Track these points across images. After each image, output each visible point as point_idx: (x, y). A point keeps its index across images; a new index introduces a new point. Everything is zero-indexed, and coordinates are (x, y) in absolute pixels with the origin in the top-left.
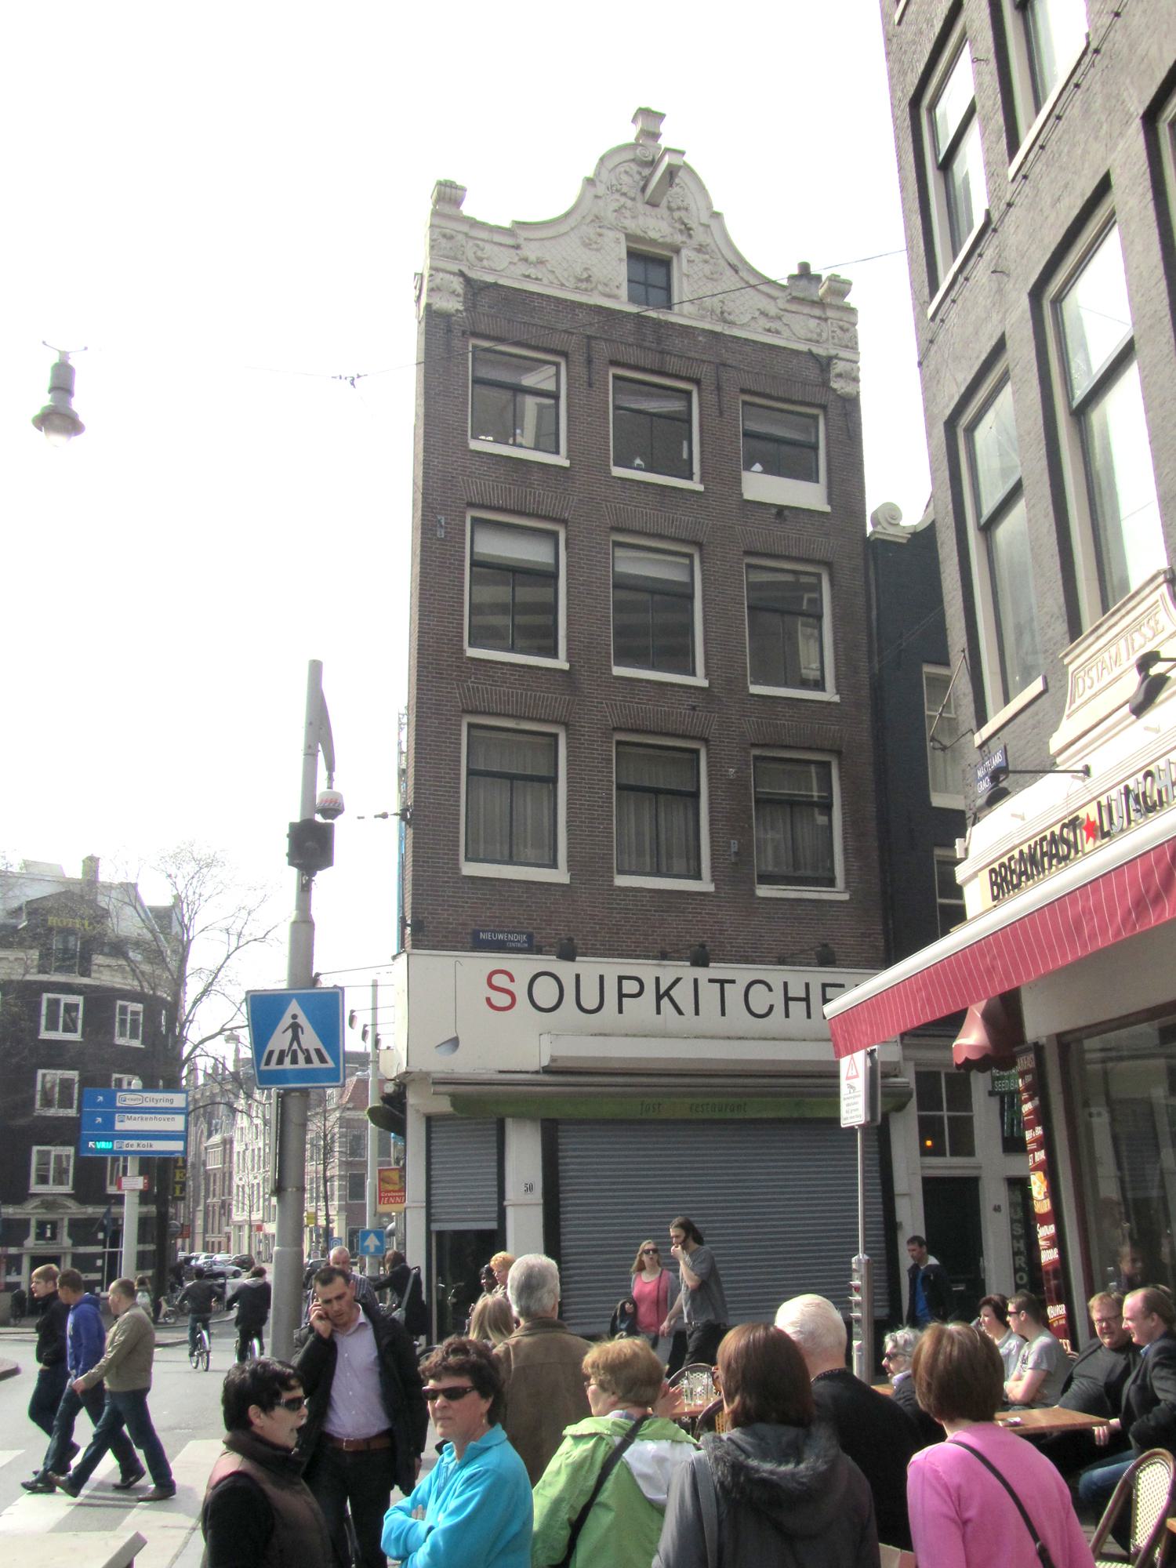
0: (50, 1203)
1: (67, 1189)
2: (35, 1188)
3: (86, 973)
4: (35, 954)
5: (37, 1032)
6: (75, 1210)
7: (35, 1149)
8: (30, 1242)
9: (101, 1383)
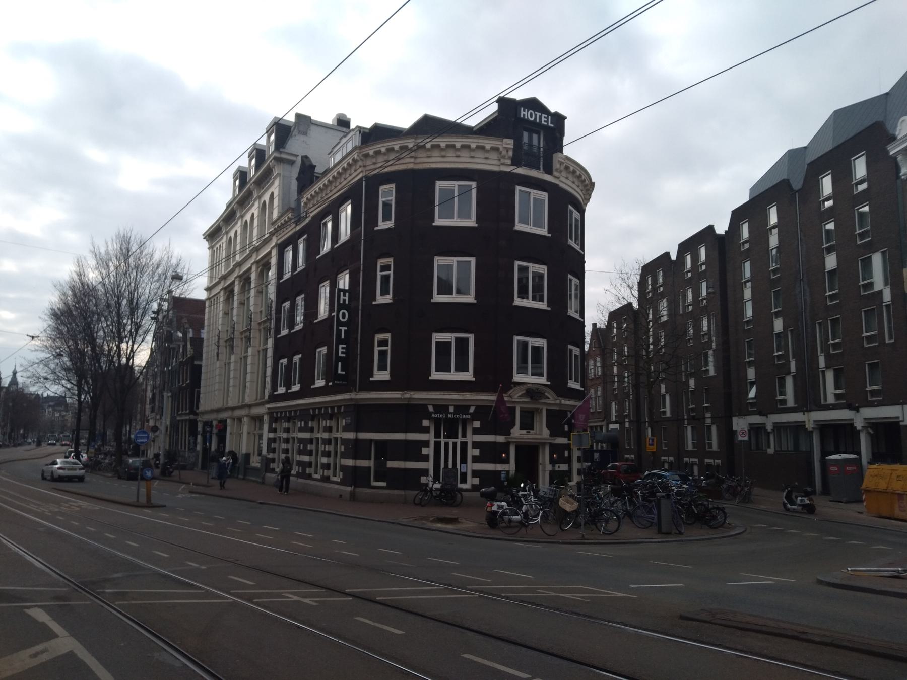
0: (533, 393)
1: (542, 380)
2: (517, 378)
3: (549, 170)
4: (509, 143)
5: (514, 225)
6: (552, 399)
7: (516, 338)
8: (517, 432)
9: (469, 406)
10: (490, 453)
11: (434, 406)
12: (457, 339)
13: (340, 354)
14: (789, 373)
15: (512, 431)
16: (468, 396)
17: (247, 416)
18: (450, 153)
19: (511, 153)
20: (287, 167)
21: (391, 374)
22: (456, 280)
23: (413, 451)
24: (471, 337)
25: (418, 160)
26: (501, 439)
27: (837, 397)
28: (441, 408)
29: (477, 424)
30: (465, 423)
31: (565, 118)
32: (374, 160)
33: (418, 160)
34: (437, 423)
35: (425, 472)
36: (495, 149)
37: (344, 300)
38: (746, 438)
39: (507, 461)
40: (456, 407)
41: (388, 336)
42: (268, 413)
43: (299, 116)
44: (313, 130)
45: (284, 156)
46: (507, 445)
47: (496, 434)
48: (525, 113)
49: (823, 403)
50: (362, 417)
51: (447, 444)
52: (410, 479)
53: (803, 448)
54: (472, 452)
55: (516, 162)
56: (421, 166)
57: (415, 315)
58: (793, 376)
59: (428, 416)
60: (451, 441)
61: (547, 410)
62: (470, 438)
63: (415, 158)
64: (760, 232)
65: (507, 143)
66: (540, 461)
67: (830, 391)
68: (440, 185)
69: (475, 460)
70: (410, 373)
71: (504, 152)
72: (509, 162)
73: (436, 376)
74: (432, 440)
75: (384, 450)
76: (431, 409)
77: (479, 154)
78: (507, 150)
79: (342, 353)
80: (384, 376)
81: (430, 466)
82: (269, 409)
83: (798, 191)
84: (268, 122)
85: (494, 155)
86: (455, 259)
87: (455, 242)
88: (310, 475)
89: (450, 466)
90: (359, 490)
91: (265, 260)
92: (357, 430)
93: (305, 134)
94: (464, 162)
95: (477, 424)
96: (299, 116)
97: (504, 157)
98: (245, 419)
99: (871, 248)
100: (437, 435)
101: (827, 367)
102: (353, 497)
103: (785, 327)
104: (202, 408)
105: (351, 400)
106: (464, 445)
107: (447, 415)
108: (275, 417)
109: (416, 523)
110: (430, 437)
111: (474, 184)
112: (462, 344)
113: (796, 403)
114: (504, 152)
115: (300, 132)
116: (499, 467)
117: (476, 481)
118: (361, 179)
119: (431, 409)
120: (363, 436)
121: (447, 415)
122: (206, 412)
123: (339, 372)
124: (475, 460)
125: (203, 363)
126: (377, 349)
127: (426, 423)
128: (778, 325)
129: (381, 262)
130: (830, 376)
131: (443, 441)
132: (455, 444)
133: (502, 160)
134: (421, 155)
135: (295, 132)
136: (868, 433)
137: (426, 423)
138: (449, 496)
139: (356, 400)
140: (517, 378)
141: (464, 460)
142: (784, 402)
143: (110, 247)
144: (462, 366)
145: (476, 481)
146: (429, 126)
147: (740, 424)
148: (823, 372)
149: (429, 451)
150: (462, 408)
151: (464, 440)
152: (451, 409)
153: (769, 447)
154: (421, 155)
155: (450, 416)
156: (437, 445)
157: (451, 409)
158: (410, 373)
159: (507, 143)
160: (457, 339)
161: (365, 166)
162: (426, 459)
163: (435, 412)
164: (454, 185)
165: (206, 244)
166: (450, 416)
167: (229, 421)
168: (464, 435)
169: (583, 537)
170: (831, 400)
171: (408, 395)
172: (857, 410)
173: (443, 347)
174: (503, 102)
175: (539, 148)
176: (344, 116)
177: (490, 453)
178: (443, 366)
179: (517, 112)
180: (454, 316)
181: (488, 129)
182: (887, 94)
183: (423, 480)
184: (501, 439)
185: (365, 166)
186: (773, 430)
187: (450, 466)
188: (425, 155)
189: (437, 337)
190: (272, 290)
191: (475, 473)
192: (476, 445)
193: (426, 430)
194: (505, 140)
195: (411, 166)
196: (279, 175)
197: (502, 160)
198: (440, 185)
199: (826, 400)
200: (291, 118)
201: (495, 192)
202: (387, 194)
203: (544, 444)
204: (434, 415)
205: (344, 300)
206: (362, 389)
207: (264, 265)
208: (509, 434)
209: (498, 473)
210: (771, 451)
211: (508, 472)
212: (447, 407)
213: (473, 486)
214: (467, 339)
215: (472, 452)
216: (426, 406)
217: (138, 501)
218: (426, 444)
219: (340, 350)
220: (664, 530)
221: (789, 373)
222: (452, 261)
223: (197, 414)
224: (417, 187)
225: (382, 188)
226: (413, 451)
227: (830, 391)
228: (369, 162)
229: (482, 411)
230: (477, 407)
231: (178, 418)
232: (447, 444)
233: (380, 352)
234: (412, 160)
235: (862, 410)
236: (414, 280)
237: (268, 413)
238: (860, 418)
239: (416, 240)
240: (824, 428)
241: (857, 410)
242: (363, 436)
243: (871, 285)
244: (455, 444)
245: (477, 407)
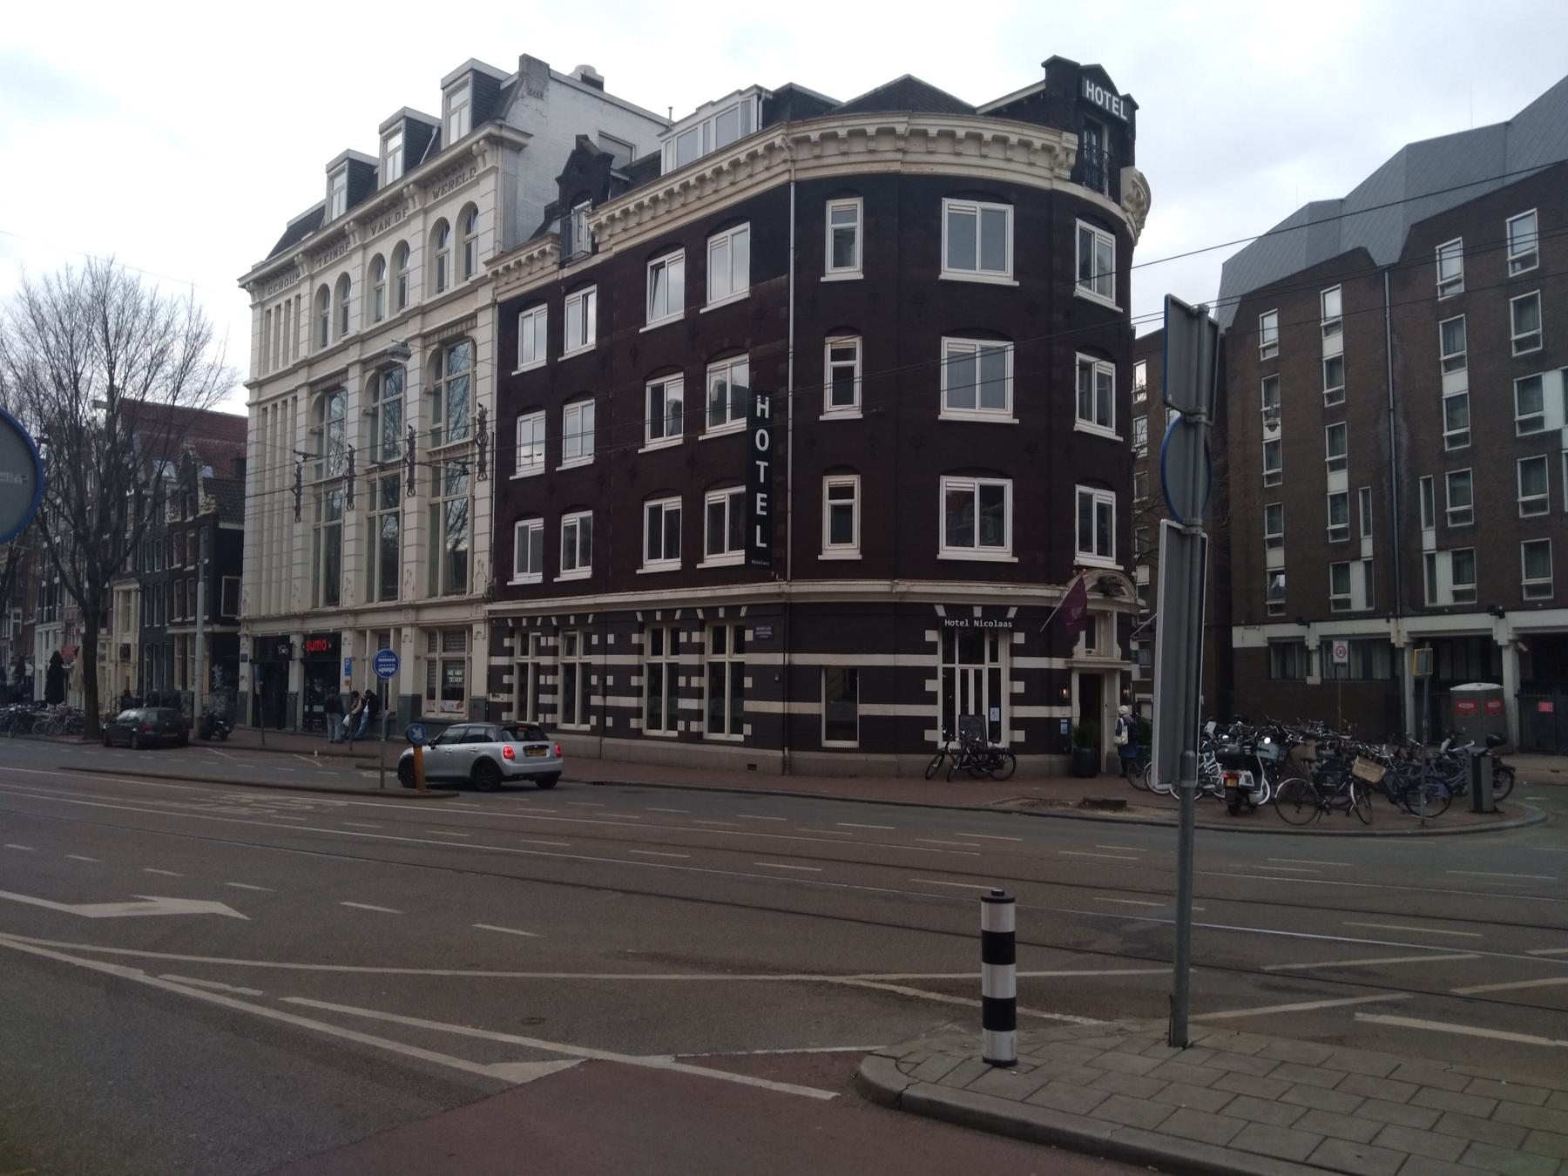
8: (1080, 650)
10: (1044, 688)
11: (946, 607)
12: (983, 488)
13: (759, 512)
14: (1358, 558)
15: (1076, 649)
16: (1010, 590)
17: (412, 625)
18: (944, 146)
19: (1072, 160)
20: (510, 155)
21: (863, 550)
22: (977, 386)
23: (908, 685)
24: (1008, 485)
25: (909, 158)
26: (1058, 663)
27: (1457, 595)
28: (959, 610)
29: (1020, 638)
30: (995, 634)
31: (582, 140)
32: (817, 151)
33: (909, 158)
34: (948, 635)
35: (930, 723)
36: (1048, 149)
37: (763, 411)
38: (1345, 660)
39: (1066, 702)
40: (985, 608)
41: (853, 480)
42: (489, 621)
43: (527, 61)
44: (554, 92)
45: (506, 134)
46: (1068, 672)
47: (1050, 655)
48: (1092, 91)
49: (1427, 603)
50: (798, 624)
51: (964, 674)
52: (907, 735)
53: (1380, 672)
54: (1007, 687)
55: (1077, 178)
56: (914, 169)
57: (905, 443)
58: (1368, 564)
59: (937, 623)
60: (971, 668)
61: (1119, 614)
62: (1004, 663)
63: (904, 152)
64: (1304, 330)
65: (1068, 141)
66: (1106, 700)
67: (1445, 585)
68: (949, 205)
69: (1016, 700)
70: (900, 541)
71: (1062, 157)
72: (1067, 174)
73: (947, 552)
74: (941, 666)
75: (851, 684)
76: (941, 611)
77: (1020, 156)
78: (1067, 151)
79: (762, 508)
80: (850, 552)
81: (937, 710)
82: (490, 612)
83: (1390, 268)
84: (453, 62)
85: (1043, 160)
86: (979, 344)
87: (977, 311)
88: (700, 734)
89: (972, 711)
90: (798, 755)
91: (459, 329)
92: (791, 649)
93: (540, 96)
94: (994, 167)
95: (1020, 638)
96: (527, 61)
97: (1060, 165)
98: (406, 631)
99: (1544, 362)
100: (948, 657)
101: (1439, 548)
102: (788, 767)
103: (1353, 486)
104: (245, 612)
105: (779, 595)
106: (995, 675)
107: (971, 623)
108: (499, 628)
109: (1025, 809)
110: (935, 660)
111: (1009, 210)
112: (992, 497)
113: (1369, 603)
114: (1062, 157)
115: (530, 92)
116: (1058, 712)
117: (1020, 736)
118: (787, 185)
119: (941, 611)
120: (801, 659)
121: (971, 623)
122: (252, 621)
123: (759, 544)
124: (1016, 700)
125: (249, 527)
126: (828, 504)
127: (931, 636)
128: (1338, 482)
129: (831, 344)
130: (1444, 564)
131: (958, 667)
132: (978, 674)
133: (1057, 171)
134: (914, 149)
135: (523, 91)
136: (1520, 652)
137: (931, 636)
138: (981, 764)
139: (790, 595)
140: (1082, 558)
141: (995, 701)
142: (1347, 603)
143: (56, 291)
144: (993, 537)
145: (1020, 736)
146: (908, 96)
147: (1245, 638)
148: (1431, 558)
149: (934, 686)
150: (995, 611)
151: (994, 665)
152: (978, 612)
153: (1309, 673)
154: (914, 149)
155: (976, 623)
156: (949, 674)
157: (978, 612)
158: (900, 541)
159: (1068, 141)
160: (983, 488)
161: (794, 161)
162: (931, 699)
163: (950, 616)
164: (976, 207)
165: (246, 298)
166: (976, 623)
167: (345, 635)
168: (994, 658)
169: (1423, 824)
170: (1445, 598)
171: (903, 586)
172: (1501, 615)
173: (960, 501)
174: (1056, 67)
175: (1101, 154)
176: (592, 69)
177: (1044, 688)
178: (961, 537)
179: (1080, 88)
180: (976, 447)
181: (1017, 109)
182: (1507, 124)
183: (929, 735)
184: (1058, 663)
185: (794, 161)
186: (1320, 647)
187: (972, 711)
188: (923, 149)
189: (949, 484)
190: (485, 391)
191: (1016, 723)
192: (1016, 674)
193: (930, 649)
194: (1066, 135)
195: (895, 167)
196: (494, 169)
197: (1057, 171)
198: (949, 205)
199: (1433, 597)
200: (511, 67)
201: (1046, 227)
202: (845, 215)
203: (1112, 672)
204: (949, 623)
205: (763, 411)
206: (798, 575)
207: (448, 343)
208: (1071, 655)
209: (1055, 722)
210: (1314, 679)
211: (1070, 719)
212: (970, 608)
213: (1012, 743)
214: (1001, 489)
215: (934, 686)
216: (970, 608)
217: (382, 786)
218: (931, 672)
219: (759, 504)
220: (1486, 805)
221: (1358, 558)
222: (973, 345)
223: (238, 624)
224: (903, 208)
225: (832, 206)
226: (908, 685)
227: (1445, 585)
228: (804, 153)
229: (1030, 616)
230: (1021, 609)
231: (171, 631)
232: (964, 674)
233: (835, 509)
234: (899, 156)
235: (1508, 615)
236: (904, 382)
237: (489, 621)
238: (1503, 630)
239: (907, 308)
240: (1439, 645)
241: (1501, 615)
242: (801, 659)
243: (1539, 422)
244: (978, 674)
245: (1021, 609)
